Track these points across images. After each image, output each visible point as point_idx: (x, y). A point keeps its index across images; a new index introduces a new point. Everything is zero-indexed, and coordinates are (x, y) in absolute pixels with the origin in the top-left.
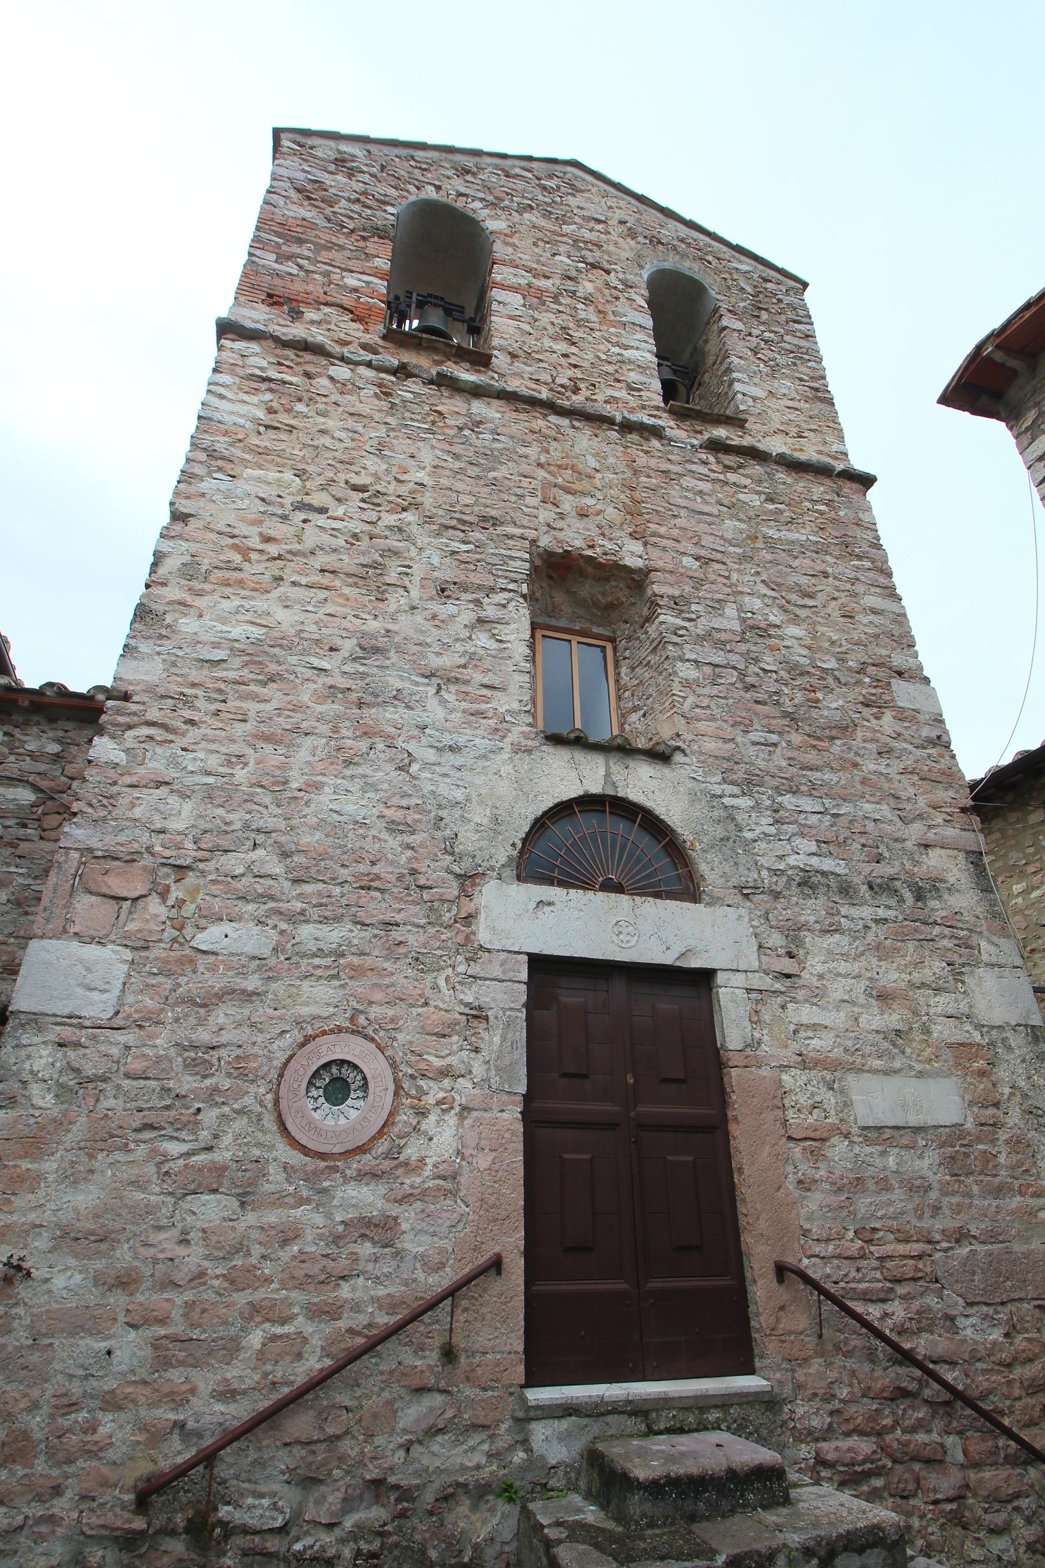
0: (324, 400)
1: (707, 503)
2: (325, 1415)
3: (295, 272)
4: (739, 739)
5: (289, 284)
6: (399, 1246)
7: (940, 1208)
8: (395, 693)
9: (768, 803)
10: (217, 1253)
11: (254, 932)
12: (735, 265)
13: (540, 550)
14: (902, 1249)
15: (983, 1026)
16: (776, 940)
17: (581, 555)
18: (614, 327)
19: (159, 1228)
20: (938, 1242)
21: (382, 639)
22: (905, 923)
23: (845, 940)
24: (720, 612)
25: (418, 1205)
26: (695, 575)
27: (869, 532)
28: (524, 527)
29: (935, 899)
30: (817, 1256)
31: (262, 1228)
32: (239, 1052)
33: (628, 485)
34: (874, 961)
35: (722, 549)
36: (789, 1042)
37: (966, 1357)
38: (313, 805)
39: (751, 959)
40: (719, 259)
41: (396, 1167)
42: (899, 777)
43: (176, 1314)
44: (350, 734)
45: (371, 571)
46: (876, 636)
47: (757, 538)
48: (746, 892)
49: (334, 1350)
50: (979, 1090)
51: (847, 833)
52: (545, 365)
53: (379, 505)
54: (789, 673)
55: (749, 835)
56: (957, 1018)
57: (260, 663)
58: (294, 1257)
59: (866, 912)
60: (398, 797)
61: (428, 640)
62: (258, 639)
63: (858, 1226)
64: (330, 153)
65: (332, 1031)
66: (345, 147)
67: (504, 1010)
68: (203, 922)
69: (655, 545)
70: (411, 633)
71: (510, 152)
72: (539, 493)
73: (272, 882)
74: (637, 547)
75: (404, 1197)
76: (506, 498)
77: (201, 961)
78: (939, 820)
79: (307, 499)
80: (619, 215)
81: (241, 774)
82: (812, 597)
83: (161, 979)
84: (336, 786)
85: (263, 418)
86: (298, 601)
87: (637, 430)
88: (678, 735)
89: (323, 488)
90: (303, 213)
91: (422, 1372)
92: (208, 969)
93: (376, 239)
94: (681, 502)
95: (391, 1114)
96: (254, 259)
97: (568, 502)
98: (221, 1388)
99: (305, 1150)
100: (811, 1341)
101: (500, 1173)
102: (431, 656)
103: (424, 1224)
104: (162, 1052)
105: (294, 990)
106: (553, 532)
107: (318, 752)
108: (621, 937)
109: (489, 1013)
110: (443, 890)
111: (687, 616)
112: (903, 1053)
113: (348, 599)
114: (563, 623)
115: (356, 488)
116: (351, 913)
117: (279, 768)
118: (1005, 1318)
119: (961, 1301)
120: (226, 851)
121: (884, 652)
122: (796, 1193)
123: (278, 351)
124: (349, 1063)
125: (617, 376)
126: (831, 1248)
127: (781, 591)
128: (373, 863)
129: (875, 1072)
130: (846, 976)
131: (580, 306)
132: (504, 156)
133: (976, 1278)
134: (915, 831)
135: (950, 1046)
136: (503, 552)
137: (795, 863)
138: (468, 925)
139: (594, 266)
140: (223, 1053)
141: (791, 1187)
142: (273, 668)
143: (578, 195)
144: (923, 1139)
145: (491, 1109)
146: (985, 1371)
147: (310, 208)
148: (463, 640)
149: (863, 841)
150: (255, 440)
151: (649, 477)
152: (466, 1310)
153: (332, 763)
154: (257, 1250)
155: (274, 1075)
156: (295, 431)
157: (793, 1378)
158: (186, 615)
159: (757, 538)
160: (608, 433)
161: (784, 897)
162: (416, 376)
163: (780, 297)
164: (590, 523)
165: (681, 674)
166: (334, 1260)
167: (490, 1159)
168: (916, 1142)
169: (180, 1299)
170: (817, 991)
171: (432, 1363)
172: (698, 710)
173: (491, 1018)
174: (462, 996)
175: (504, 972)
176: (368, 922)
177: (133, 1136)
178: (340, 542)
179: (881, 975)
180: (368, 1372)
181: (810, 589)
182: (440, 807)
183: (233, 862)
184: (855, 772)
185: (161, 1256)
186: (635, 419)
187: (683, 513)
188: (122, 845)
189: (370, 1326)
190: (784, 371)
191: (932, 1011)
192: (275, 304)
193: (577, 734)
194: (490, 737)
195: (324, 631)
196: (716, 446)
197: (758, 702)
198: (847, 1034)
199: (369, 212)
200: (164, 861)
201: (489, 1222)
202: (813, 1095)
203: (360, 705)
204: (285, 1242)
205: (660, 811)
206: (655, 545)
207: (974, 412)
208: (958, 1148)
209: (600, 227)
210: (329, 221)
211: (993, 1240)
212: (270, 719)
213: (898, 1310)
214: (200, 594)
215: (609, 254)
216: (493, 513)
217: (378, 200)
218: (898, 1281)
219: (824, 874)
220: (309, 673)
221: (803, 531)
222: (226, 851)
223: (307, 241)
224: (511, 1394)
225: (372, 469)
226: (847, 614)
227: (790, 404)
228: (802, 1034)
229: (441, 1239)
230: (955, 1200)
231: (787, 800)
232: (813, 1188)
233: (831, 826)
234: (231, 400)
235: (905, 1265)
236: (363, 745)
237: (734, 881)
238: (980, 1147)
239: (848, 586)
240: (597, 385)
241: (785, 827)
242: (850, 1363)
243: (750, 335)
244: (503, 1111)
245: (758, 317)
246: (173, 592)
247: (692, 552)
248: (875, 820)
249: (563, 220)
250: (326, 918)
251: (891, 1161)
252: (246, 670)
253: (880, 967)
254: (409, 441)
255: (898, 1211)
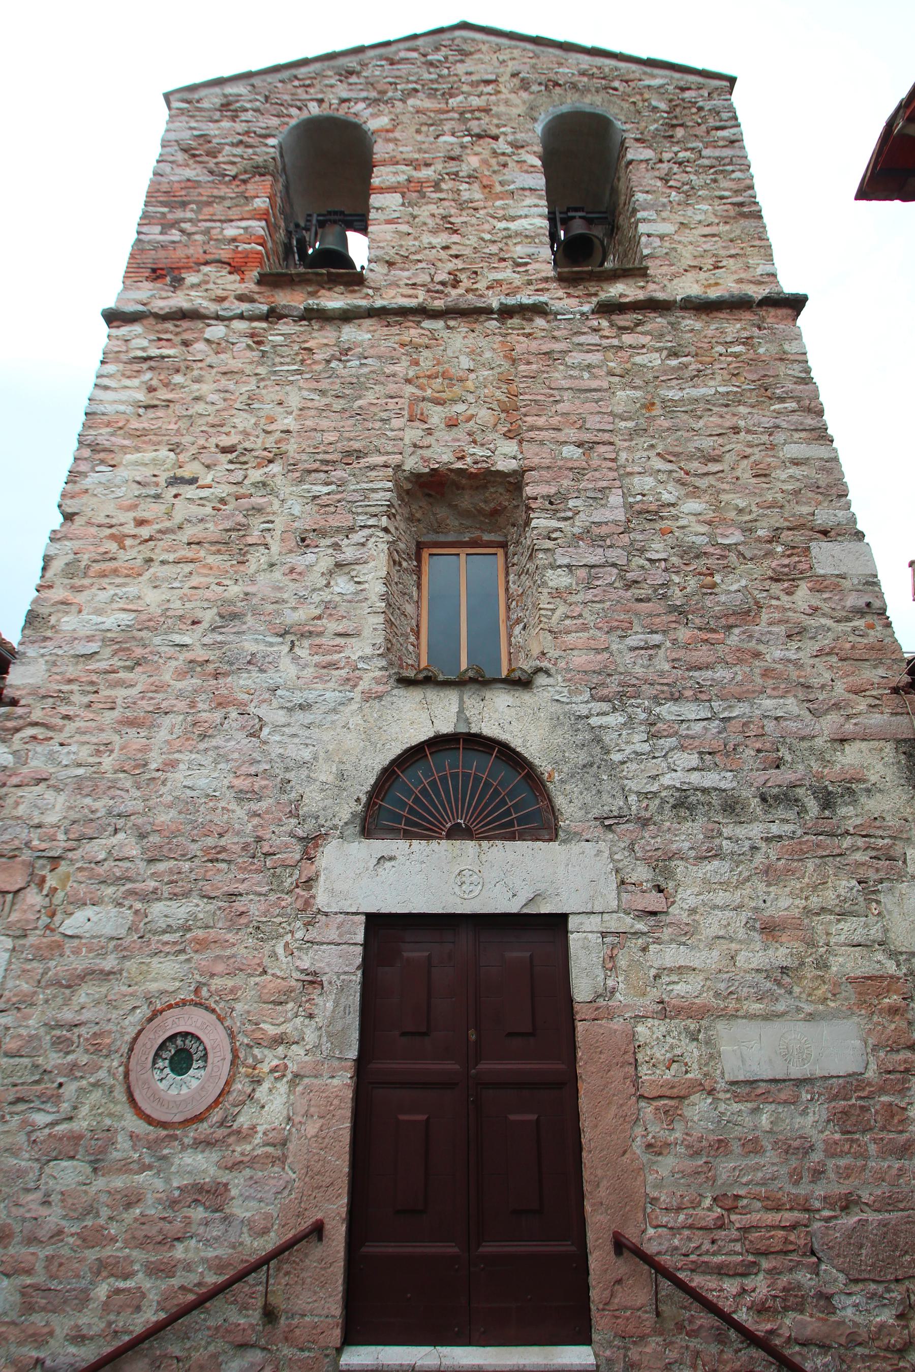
0: (200, 365)
1: (596, 377)
2: (158, 1363)
3: (177, 238)
4: (614, 647)
5: (171, 254)
6: (228, 1211)
7: (823, 1172)
8: (249, 658)
9: (643, 716)
10: (72, 1214)
11: (112, 914)
12: (647, 83)
13: (407, 474)
14: (771, 1218)
15: (901, 953)
16: (641, 873)
17: (449, 469)
18: (502, 199)
19: (28, 1190)
20: (818, 1210)
21: (239, 604)
22: (806, 838)
23: (726, 866)
24: (603, 502)
25: (248, 1172)
26: (576, 464)
27: (795, 366)
28: (388, 453)
29: (847, 804)
30: (665, 1226)
31: (109, 1192)
32: (96, 1029)
33: (503, 378)
34: (762, 887)
35: (610, 427)
36: (648, 989)
37: (843, 1340)
38: (169, 784)
39: (609, 897)
40: (627, 82)
41: (229, 1135)
42: (812, 661)
43: (39, 1267)
44: (206, 707)
45: (234, 535)
46: (797, 492)
47: (653, 404)
48: (607, 823)
49: (168, 1305)
50: (888, 1031)
51: (740, 739)
52: (423, 265)
53: (245, 463)
54: (682, 557)
55: (616, 757)
56: (866, 946)
57: (128, 649)
58: (136, 1220)
59: (756, 830)
60: (247, 765)
61: (285, 596)
62: (128, 626)
63: (717, 1193)
64: (216, 100)
65: (177, 1004)
66: (230, 90)
67: (338, 974)
68: (71, 908)
69: (532, 440)
70: (268, 592)
71: (392, 38)
72: (405, 413)
73: (129, 864)
74: (510, 447)
75: (235, 1164)
76: (370, 425)
77: (69, 945)
78: (862, 707)
79: (180, 473)
80: (512, 66)
81: (108, 762)
82: (718, 461)
83: (35, 964)
84: (190, 762)
85: (142, 399)
86: (165, 579)
87: (518, 312)
88: (544, 654)
89: (194, 458)
90: (189, 173)
91: (244, 1330)
92: (73, 952)
93: (257, 178)
94: (565, 383)
95: (227, 1083)
96: (142, 237)
97: (436, 415)
98: (73, 1333)
99: (149, 1120)
100: (649, 1318)
101: (327, 1140)
102: (287, 612)
103: (252, 1191)
104: (33, 1032)
105: (145, 968)
106: (420, 452)
107: (175, 730)
108: (464, 887)
109: (324, 979)
110: (285, 856)
111: (563, 515)
112: (791, 993)
113: (211, 568)
114: (451, 538)
115: (225, 450)
116: (199, 887)
117: (140, 751)
118: (899, 1297)
119: (841, 1277)
120: (91, 839)
121: (805, 510)
122: (645, 1158)
123: (159, 327)
124: (192, 1035)
125: (502, 255)
126: (682, 1217)
127: (679, 462)
128: (221, 835)
129: (752, 1017)
130: (722, 908)
131: (464, 186)
132: (387, 44)
133: (863, 1251)
134: (830, 723)
135: (852, 981)
136: (365, 486)
137: (670, 783)
138: (309, 888)
139: (479, 136)
140: (83, 1030)
141: (638, 1151)
142: (139, 652)
143: (468, 60)
144: (807, 1092)
145: (321, 1075)
146: (864, 1358)
147: (194, 166)
148: (319, 590)
149: (758, 745)
150: (135, 424)
151: (529, 363)
152: (287, 1273)
153: (188, 739)
154: (105, 1212)
155: (125, 1049)
156: (171, 405)
157: (625, 1356)
158: (67, 613)
159: (653, 404)
160: (486, 324)
161: (655, 824)
162: (286, 316)
163: (700, 104)
164: (460, 433)
165: (551, 584)
166: (170, 1222)
167: (318, 1125)
168: (798, 1096)
169: (44, 1253)
170: (686, 929)
171: (255, 1322)
172: (568, 622)
173: (325, 984)
174: (298, 963)
175: (340, 935)
176: (213, 895)
177: (8, 1109)
178: (208, 510)
179: (768, 904)
180: (197, 1327)
181: (717, 452)
182: (287, 769)
183: (97, 849)
184: (757, 663)
185: (28, 1215)
186: (513, 302)
187: (567, 395)
188: (6, 843)
189: (199, 1284)
190: (700, 193)
191: (833, 940)
192: (158, 278)
193: (425, 673)
194: (341, 688)
195: (188, 605)
196: (608, 309)
197: (639, 600)
198: (719, 976)
199: (250, 151)
200: (39, 854)
201: (314, 1188)
202: (672, 1047)
203: (216, 676)
204: (129, 1206)
205: (516, 743)
206: (532, 440)
207: (904, 199)
208: (853, 1101)
209: (489, 89)
210: (211, 172)
211: (890, 1208)
212: (135, 703)
213: (760, 1286)
214: (79, 590)
215: (498, 116)
216: (356, 445)
217: (261, 136)
218: (766, 1254)
219: (705, 791)
220: (171, 651)
221: (712, 383)
222: (91, 839)
223: (190, 203)
224: (327, 1356)
225: (241, 427)
226: (760, 472)
227: (707, 230)
228: (665, 979)
229: (267, 1204)
230: (842, 1162)
231: (668, 710)
232: (665, 1152)
233: (719, 733)
234: (115, 389)
235: (772, 1237)
236: (217, 716)
237: (596, 812)
238: (885, 1099)
239: (765, 438)
240: (479, 271)
241: (662, 741)
242: (694, 1343)
243: (661, 161)
244: (333, 1077)
245: (671, 137)
246: (58, 594)
247: (574, 439)
248: (776, 718)
249: (450, 93)
250: (175, 895)
251: (764, 1120)
252: (116, 659)
253: (769, 893)
254: (278, 388)
255: (768, 1176)
